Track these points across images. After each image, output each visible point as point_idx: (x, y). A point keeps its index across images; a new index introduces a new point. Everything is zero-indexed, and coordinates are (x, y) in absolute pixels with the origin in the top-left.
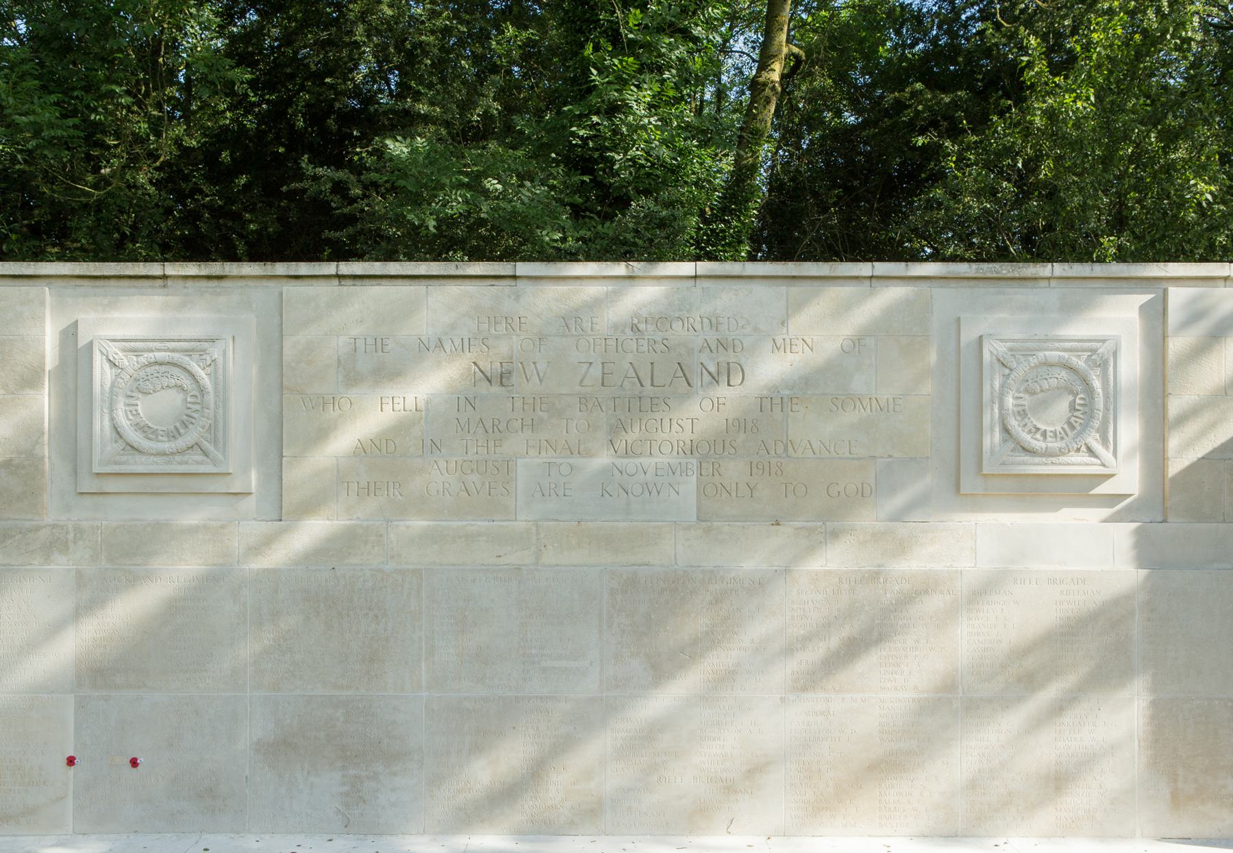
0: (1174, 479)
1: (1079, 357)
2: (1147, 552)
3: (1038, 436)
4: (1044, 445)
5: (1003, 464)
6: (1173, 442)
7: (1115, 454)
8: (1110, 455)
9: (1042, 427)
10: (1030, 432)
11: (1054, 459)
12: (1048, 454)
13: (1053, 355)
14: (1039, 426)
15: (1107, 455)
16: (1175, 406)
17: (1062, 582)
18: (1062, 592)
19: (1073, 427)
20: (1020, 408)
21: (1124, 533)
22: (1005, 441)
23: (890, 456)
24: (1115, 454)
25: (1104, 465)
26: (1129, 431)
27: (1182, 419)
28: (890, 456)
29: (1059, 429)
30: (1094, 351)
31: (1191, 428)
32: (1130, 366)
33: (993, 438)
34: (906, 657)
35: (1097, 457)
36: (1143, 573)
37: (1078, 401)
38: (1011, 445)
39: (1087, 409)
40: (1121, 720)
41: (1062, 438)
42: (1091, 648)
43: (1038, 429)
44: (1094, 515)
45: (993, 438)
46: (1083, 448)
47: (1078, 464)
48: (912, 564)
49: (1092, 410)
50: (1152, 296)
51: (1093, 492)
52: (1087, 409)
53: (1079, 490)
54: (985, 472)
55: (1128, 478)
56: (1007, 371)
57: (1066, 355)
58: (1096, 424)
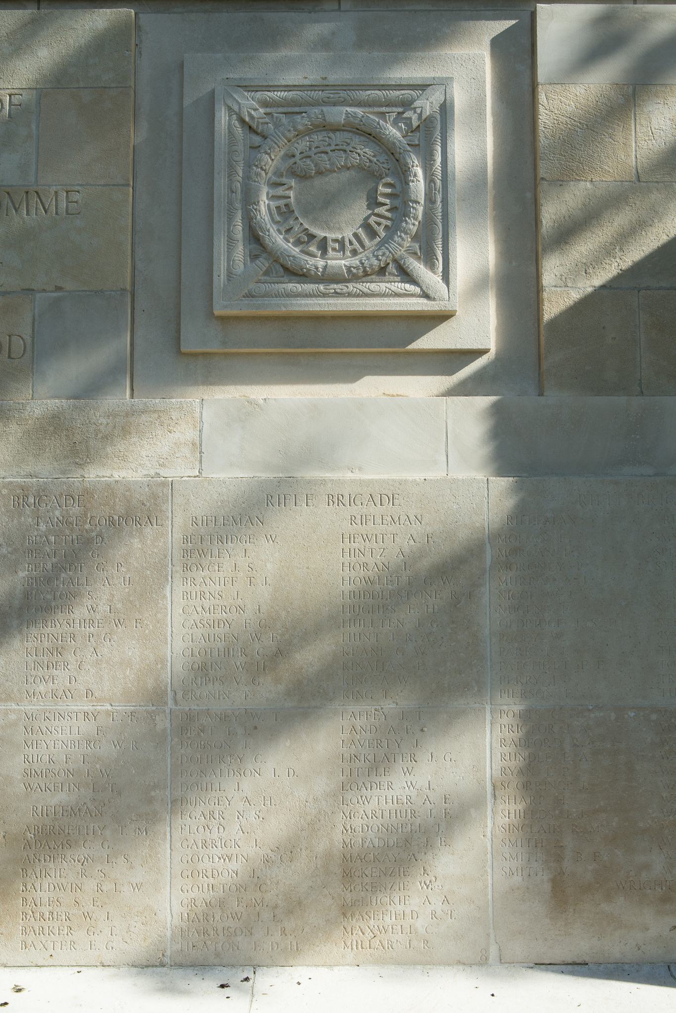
0: (553, 322)
1: (382, 115)
2: (513, 448)
3: (313, 249)
4: (321, 263)
5: (250, 295)
6: (552, 270)
7: (446, 278)
8: (439, 279)
9: (321, 233)
10: (298, 242)
11: (338, 287)
12: (329, 277)
13: (339, 114)
14: (314, 230)
15: (431, 278)
16: (552, 212)
17: (353, 501)
18: (353, 519)
19: (372, 234)
20: (281, 203)
21: (467, 421)
22: (254, 257)
23: (59, 289)
24: (446, 278)
25: (426, 296)
26: (474, 252)
27: (567, 233)
28: (59, 289)
29: (348, 234)
30: (407, 104)
31: (584, 247)
32: (473, 147)
33: (231, 257)
34: (73, 637)
35: (414, 281)
36: (502, 483)
37: (381, 189)
38: (263, 263)
39: (397, 203)
40: (474, 754)
41: (354, 253)
42: (404, 643)
43: (312, 237)
44: (420, 388)
45: (231, 257)
46: (392, 268)
47: (390, 298)
48: (129, 467)
49: (405, 204)
50: (514, 22)
51: (410, 347)
52: (397, 203)
53: (392, 343)
54: (217, 312)
55: (478, 326)
56: (257, 140)
57: (359, 111)
58: (413, 226)
